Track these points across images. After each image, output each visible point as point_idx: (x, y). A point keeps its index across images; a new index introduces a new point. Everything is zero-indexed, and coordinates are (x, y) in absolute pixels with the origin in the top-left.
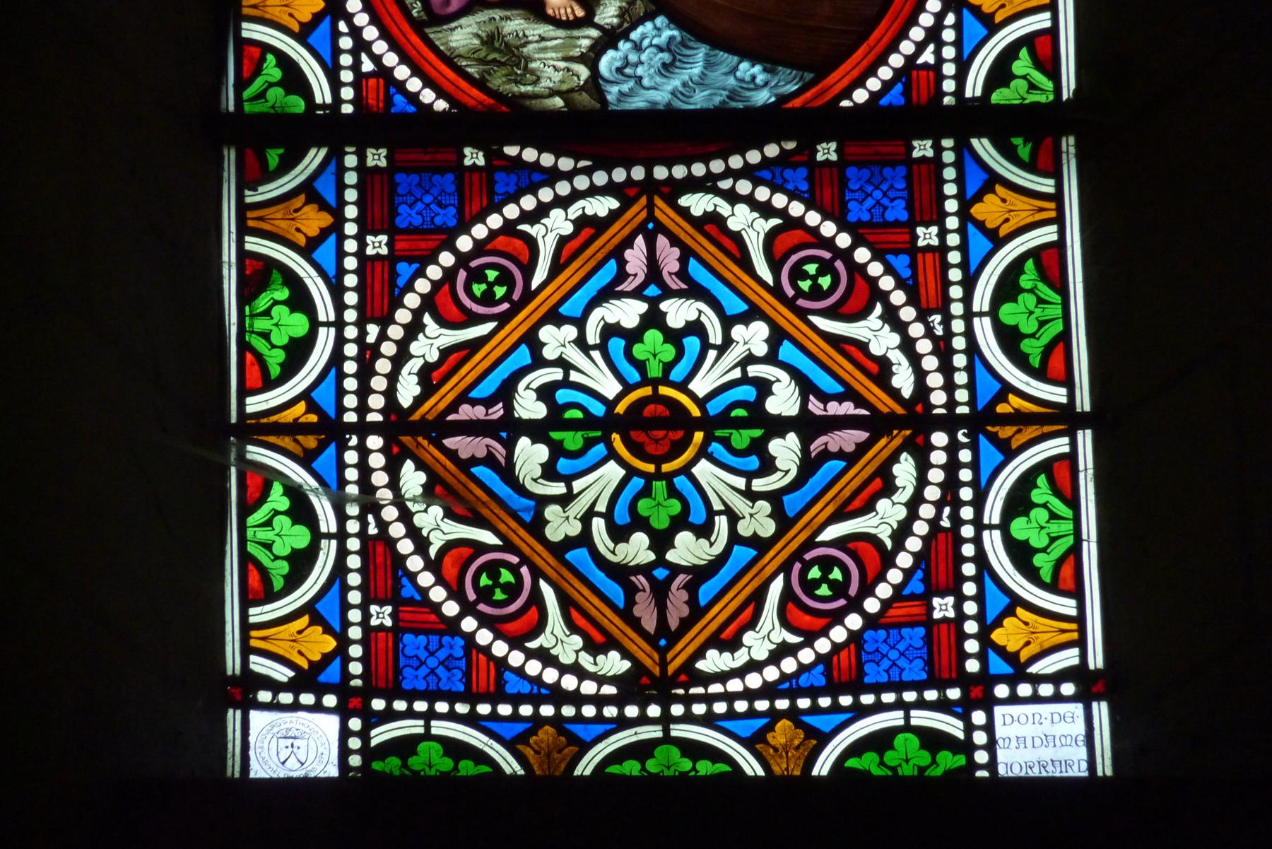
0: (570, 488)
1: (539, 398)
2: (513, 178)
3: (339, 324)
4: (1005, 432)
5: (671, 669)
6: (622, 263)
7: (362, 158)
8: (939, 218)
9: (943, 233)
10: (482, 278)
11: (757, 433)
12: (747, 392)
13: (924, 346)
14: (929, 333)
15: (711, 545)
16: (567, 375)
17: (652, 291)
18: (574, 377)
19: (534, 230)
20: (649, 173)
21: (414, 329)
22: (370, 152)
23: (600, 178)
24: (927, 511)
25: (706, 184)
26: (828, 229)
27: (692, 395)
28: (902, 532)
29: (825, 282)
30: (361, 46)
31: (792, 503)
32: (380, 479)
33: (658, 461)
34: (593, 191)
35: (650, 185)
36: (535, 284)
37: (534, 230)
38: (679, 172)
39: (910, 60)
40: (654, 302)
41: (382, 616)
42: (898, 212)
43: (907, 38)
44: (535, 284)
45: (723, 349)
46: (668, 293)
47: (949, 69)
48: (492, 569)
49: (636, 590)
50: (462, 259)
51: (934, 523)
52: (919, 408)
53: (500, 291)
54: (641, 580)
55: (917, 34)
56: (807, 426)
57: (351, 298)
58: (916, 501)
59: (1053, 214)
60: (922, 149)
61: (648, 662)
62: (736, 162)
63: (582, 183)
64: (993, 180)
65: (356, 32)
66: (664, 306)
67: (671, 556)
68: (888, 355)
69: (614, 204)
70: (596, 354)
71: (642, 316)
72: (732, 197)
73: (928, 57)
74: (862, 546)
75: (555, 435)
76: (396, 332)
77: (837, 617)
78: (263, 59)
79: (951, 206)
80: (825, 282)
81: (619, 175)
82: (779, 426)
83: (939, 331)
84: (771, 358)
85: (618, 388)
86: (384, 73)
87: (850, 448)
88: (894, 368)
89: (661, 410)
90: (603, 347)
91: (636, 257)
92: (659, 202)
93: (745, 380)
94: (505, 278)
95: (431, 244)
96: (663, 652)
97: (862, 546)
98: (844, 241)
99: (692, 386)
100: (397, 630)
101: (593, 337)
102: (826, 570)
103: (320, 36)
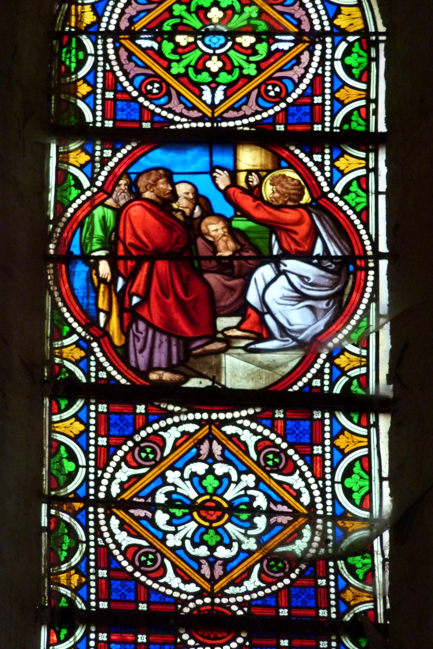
0: (246, 492)
1: (256, 524)
3: (87, 466)
5: (207, 427)
12: (246, 499)
13: (106, 535)
17: (213, 85)
18: (243, 531)
22: (320, 129)
23: (191, 416)
24: (107, 475)
25: (233, 422)
27: (225, 500)
28: (118, 468)
29: (143, 558)
31: (159, 481)
32: (102, 522)
34: (188, 421)
35: (209, 421)
36: (165, 454)
38: (222, 416)
40: (211, 465)
41: (317, 450)
44: (165, 454)
45: (237, 483)
46: (206, 558)
49: (221, 456)
50: (136, 444)
51: (104, 471)
53: (151, 456)
56: (269, 513)
59: (366, 444)
61: (206, 588)
63: (184, 418)
64: (344, 429)
65: (97, 359)
67: (215, 554)
68: (120, 531)
71: (206, 470)
72: (242, 427)
74: (134, 464)
75: (172, 511)
77: (144, 440)
81: (198, 416)
89: (213, 504)
93: (246, 495)
94: (154, 452)
95: (299, 582)
96: (210, 432)
97: (134, 464)
99: (225, 496)
100: (109, 579)
101: (186, 476)
102: (147, 457)
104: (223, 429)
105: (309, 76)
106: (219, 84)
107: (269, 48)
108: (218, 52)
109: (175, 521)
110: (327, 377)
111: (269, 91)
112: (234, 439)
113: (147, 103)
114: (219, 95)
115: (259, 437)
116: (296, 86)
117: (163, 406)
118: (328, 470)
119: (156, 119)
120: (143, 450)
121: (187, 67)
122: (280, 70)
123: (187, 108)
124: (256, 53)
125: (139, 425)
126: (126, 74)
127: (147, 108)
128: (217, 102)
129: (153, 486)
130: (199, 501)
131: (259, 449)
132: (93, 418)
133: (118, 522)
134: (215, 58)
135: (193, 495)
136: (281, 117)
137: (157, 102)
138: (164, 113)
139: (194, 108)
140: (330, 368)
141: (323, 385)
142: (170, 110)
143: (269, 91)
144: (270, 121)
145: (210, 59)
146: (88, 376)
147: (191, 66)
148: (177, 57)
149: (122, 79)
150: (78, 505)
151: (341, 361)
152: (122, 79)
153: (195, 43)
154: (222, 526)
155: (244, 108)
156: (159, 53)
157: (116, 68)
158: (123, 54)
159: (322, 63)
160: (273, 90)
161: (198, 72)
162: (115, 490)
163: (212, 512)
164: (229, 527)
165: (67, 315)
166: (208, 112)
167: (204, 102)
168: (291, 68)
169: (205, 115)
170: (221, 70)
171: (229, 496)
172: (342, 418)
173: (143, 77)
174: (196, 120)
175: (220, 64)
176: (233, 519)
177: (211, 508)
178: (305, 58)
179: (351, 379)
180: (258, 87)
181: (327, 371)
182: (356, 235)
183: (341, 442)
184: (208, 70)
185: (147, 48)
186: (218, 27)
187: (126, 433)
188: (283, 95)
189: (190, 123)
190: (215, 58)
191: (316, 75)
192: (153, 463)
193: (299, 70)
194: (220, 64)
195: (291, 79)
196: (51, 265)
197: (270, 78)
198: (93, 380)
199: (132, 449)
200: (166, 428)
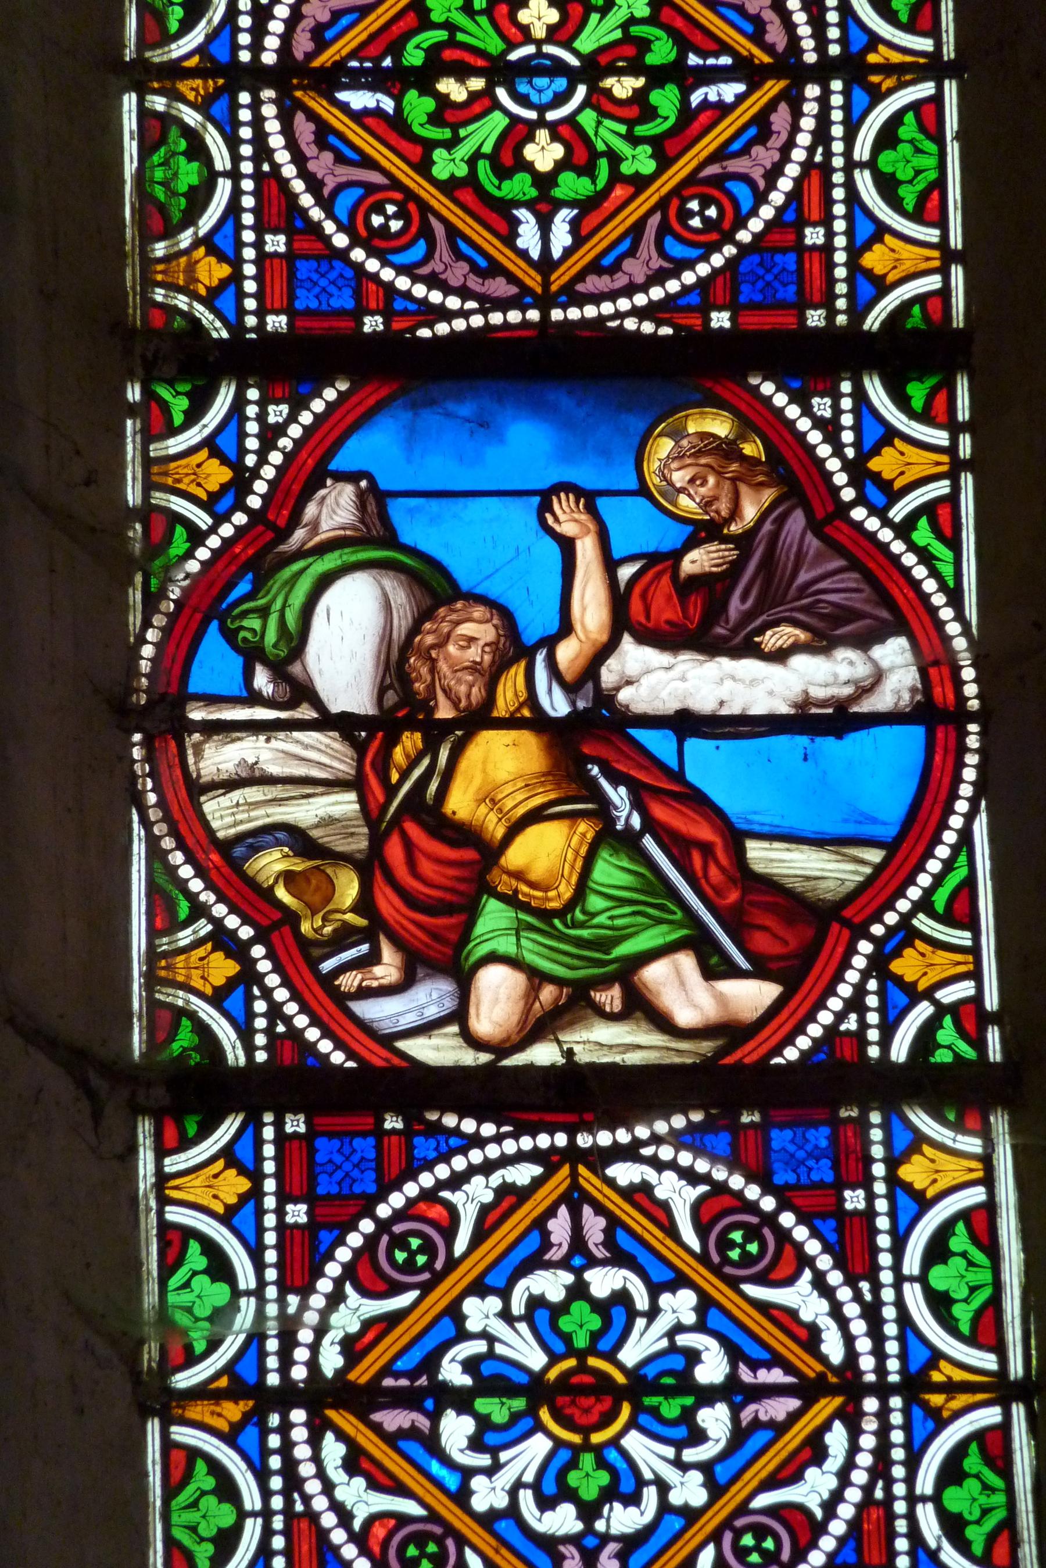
2: (432, 1143)
3: (912, 1499)
4: (936, 1399)
6: (546, 1234)
7: (279, 1125)
8: (866, 1182)
9: (871, 1197)
10: (405, 1247)
11: (640, 82)
12: (678, 1362)
14: (858, 1297)
15: (528, 1288)
16: (678, 1454)
19: (456, 1198)
20: (572, 1140)
21: (336, 1299)
22: (289, 1118)
25: (629, 1153)
26: (753, 1192)
27: (620, 1366)
30: (275, 1012)
33: (586, 1431)
35: (572, 1155)
37: (456, 1198)
38: (604, 1139)
39: (831, 1031)
40: (589, 1529)
42: (824, 1172)
43: (962, 781)
45: (518, 1485)
47: (873, 1035)
48: (420, 1539)
50: (383, 1226)
52: (849, 1374)
53: (421, 1260)
54: (600, 1253)
55: (835, 1004)
57: (271, 1256)
58: (321, 1331)
60: (277, 322)
62: (460, 325)
65: (838, 451)
66: (579, 1526)
67: (568, 1278)
69: (537, 1170)
70: (648, 1475)
73: (851, 1023)
76: (317, 1301)
77: (399, 1216)
78: (178, 1025)
79: (879, 1170)
80: (753, 1248)
81: (543, 1141)
82: (707, 1396)
83: (868, 1297)
84: (467, 1473)
85: (625, 1442)
86: (295, 1035)
87: (781, 1416)
88: (824, 1336)
89: (587, 1379)
90: (641, 1483)
91: (560, 1227)
92: (582, 1169)
98: (768, 1204)
101: (518, 1307)
103: (235, 1001)
104: (611, 1171)
105: (792, 170)
106: (559, 204)
107: (685, 101)
108: (551, 116)
109: (491, 1438)
110: (252, 427)
111: (691, 214)
112: (639, 1197)
113: (372, 265)
114: (561, 237)
115: (703, 1189)
116: (761, 198)
117: (666, 331)
118: (248, 202)
119: (399, 305)
120: (400, 1242)
121: (472, 161)
122: (715, 157)
123: (475, 269)
124: (650, 113)
125: (725, 278)
126: (314, 185)
127: (375, 277)
128: (557, 253)
129: (430, 1343)
130: (552, 1375)
131: (705, 1218)
132: (843, 280)
133: (341, 1449)
134: (542, 135)
135: (535, 1359)
136: (720, 291)
137: (398, 259)
138: (419, 291)
139: (495, 269)
140: (243, 451)
141: (262, 404)
142: (433, 281)
143: (691, 214)
144: (694, 299)
145: (530, 138)
146: (860, 396)
147: (484, 156)
148: (683, 1340)
149: (307, 200)
150: (233, 1411)
151: (218, 474)
152: (307, 200)
153: (488, 92)
154: (615, 1442)
155: (628, 264)
156: (397, 123)
157: (289, 171)
158: (304, 129)
159: (822, 135)
160: (701, 213)
161: (503, 173)
162: (331, 1361)
163: (587, 1401)
164: (635, 1443)
165: (186, 872)
166: (533, 280)
167: (524, 254)
168: (745, 151)
169: (525, 290)
170: (561, 166)
171: (631, 1354)
172: (923, 1121)
173: (359, 192)
174: (503, 305)
175: (558, 151)
176: (644, 1419)
177: (582, 1390)
178: (780, 118)
179: (941, 1010)
180: (662, 205)
181: (252, 444)
182: (921, 611)
183: (913, 1172)
184: (528, 167)
185: (366, 112)
186: (549, 49)
187: (756, 259)
188: (727, 225)
189: (484, 312)
190: (542, 135)
191: (807, 166)
192: (426, 1276)
193: (765, 156)
194: (558, 151)
195: (746, 179)
196: (137, 737)
197: (691, 180)
198: (846, 387)
199: (371, 1241)
200: (457, 1181)
